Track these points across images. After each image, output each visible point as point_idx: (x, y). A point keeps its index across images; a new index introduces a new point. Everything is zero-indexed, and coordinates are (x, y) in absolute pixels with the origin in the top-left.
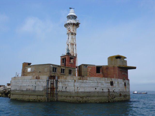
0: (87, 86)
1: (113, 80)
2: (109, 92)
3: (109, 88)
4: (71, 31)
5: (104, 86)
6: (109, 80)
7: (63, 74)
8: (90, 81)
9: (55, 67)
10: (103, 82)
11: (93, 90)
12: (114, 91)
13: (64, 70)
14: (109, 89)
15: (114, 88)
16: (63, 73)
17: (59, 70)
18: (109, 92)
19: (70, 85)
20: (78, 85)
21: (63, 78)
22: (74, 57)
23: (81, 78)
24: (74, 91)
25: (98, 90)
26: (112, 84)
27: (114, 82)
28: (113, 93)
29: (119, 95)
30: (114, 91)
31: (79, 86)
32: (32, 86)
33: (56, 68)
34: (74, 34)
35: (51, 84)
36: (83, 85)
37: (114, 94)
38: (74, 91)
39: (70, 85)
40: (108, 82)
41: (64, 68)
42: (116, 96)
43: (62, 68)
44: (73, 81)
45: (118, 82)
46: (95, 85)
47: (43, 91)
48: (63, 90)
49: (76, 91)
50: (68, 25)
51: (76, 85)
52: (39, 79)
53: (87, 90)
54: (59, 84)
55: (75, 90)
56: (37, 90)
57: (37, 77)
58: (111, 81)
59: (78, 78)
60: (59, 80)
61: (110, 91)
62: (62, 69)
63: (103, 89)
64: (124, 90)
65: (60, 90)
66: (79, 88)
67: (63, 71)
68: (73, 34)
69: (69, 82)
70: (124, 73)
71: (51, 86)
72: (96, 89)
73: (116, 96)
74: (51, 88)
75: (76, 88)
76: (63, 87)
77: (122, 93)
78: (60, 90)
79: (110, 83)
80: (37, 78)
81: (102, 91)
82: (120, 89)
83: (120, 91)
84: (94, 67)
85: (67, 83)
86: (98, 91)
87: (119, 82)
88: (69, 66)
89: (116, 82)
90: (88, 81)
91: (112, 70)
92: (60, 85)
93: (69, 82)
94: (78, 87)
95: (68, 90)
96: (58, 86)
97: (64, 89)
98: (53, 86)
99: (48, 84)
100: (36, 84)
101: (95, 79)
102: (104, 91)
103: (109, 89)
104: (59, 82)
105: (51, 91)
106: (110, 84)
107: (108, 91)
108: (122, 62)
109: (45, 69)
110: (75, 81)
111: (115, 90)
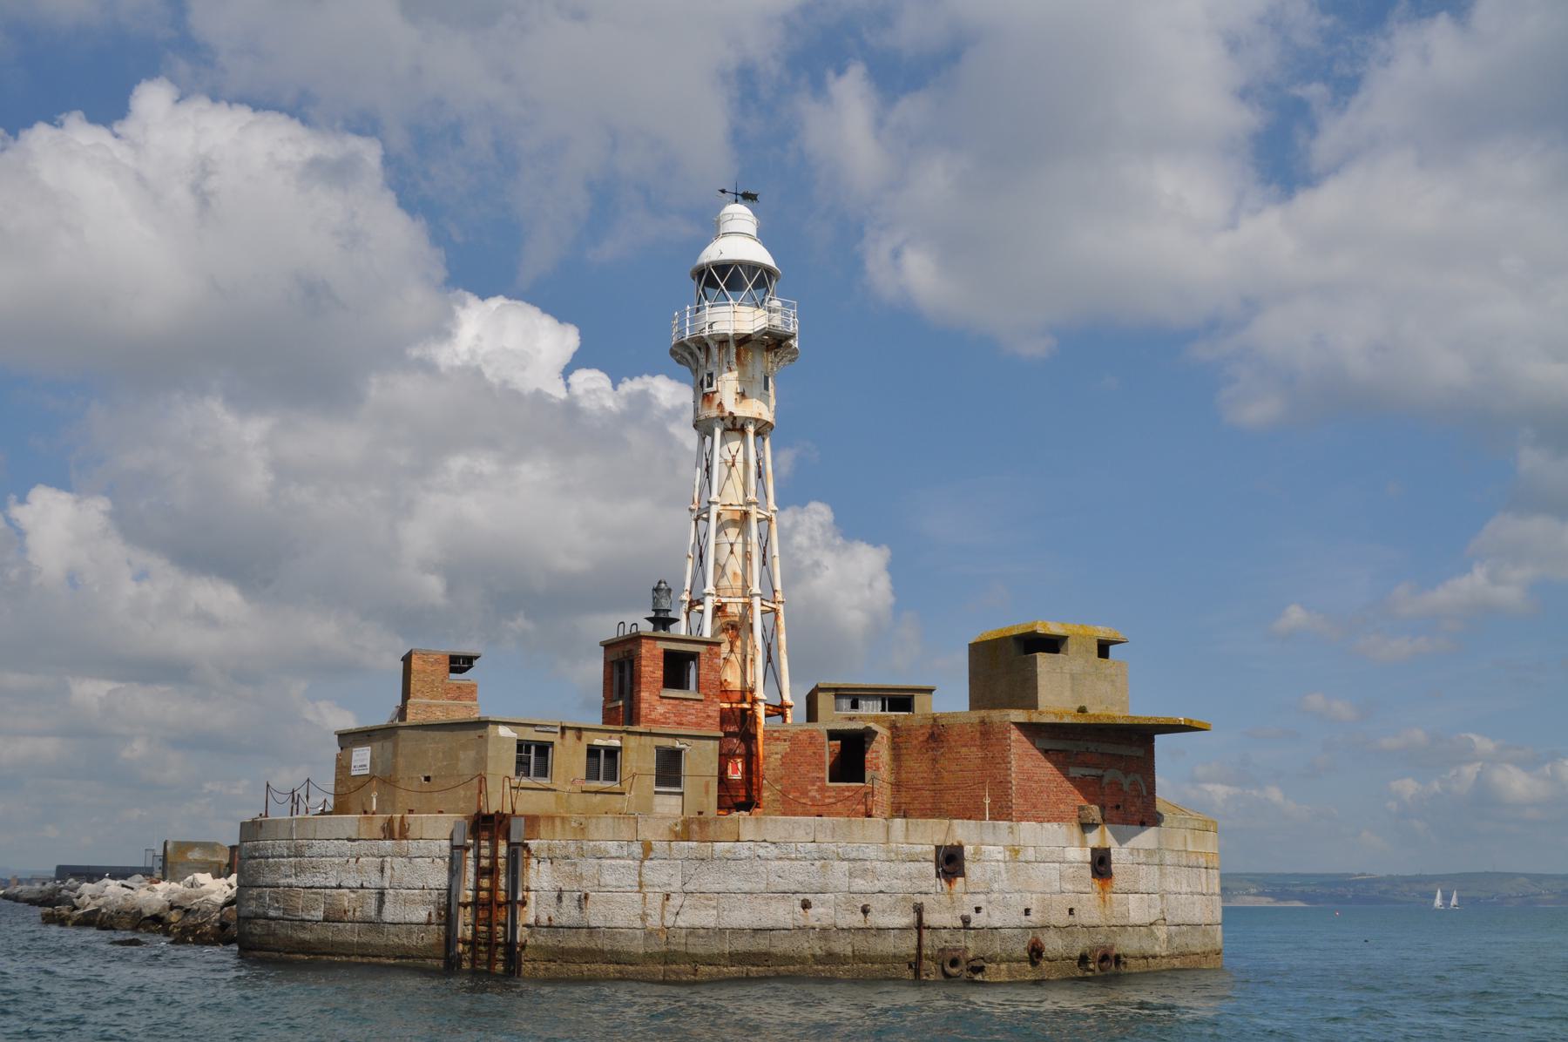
0: (734, 883)
1: (962, 832)
2: (920, 926)
3: (919, 899)
4: (720, 405)
5: (879, 885)
6: (930, 834)
7: (608, 785)
8: (762, 852)
9: (530, 735)
10: (871, 852)
11: (783, 914)
12: (966, 921)
13: (612, 753)
14: (919, 910)
15: (966, 898)
16: (612, 775)
17: (569, 760)
18: (920, 926)
19: (609, 879)
20: (665, 879)
21: (563, 828)
22: (702, 649)
23: (695, 827)
24: (638, 924)
25: (821, 914)
26: (950, 862)
27: (968, 850)
28: (960, 935)
29: (1021, 950)
30: (966, 921)
31: (676, 885)
32: (362, 887)
33: (543, 749)
34: (751, 429)
35: (480, 872)
36: (709, 881)
37: (972, 946)
38: (638, 924)
39: (618, 873)
40: (918, 848)
41: (617, 743)
42: (992, 960)
43: (597, 742)
44: (637, 849)
45: (1015, 851)
46: (798, 875)
47: (429, 923)
48: (564, 921)
49: (654, 922)
50: (702, 357)
51: (656, 881)
52: (403, 835)
53: (742, 916)
54: (532, 873)
55: (644, 917)
56: (389, 914)
57: (391, 820)
58: (940, 839)
59: (671, 830)
60: (533, 844)
61: (930, 919)
62: (593, 752)
63: (865, 911)
64: (1091, 909)
65: (544, 920)
66: (676, 901)
67: (604, 762)
68: (742, 431)
69: (600, 856)
70: (1096, 766)
71: (478, 889)
72: (806, 905)
73: (992, 960)
74: (476, 904)
75: (655, 900)
76: (566, 896)
77: (1053, 944)
78: (544, 920)
79: (932, 857)
80: (389, 832)
81: (857, 920)
82: (1032, 901)
83: (1035, 918)
84: (812, 738)
85: (588, 866)
86: (826, 922)
87: (1031, 851)
88: (654, 721)
89: (996, 852)
90: (743, 849)
91: (973, 754)
92: (539, 878)
93: (600, 856)
94: (668, 897)
95: (595, 916)
96: (528, 890)
97: (568, 914)
98: (492, 890)
99: (454, 870)
100: (382, 870)
101: (800, 834)
102: (877, 919)
103: (919, 910)
104: (533, 861)
105: (477, 921)
106: (931, 868)
107: (908, 919)
108: (1073, 677)
109: (462, 755)
110: (647, 848)
111: (984, 912)
